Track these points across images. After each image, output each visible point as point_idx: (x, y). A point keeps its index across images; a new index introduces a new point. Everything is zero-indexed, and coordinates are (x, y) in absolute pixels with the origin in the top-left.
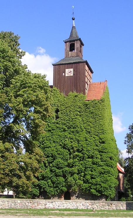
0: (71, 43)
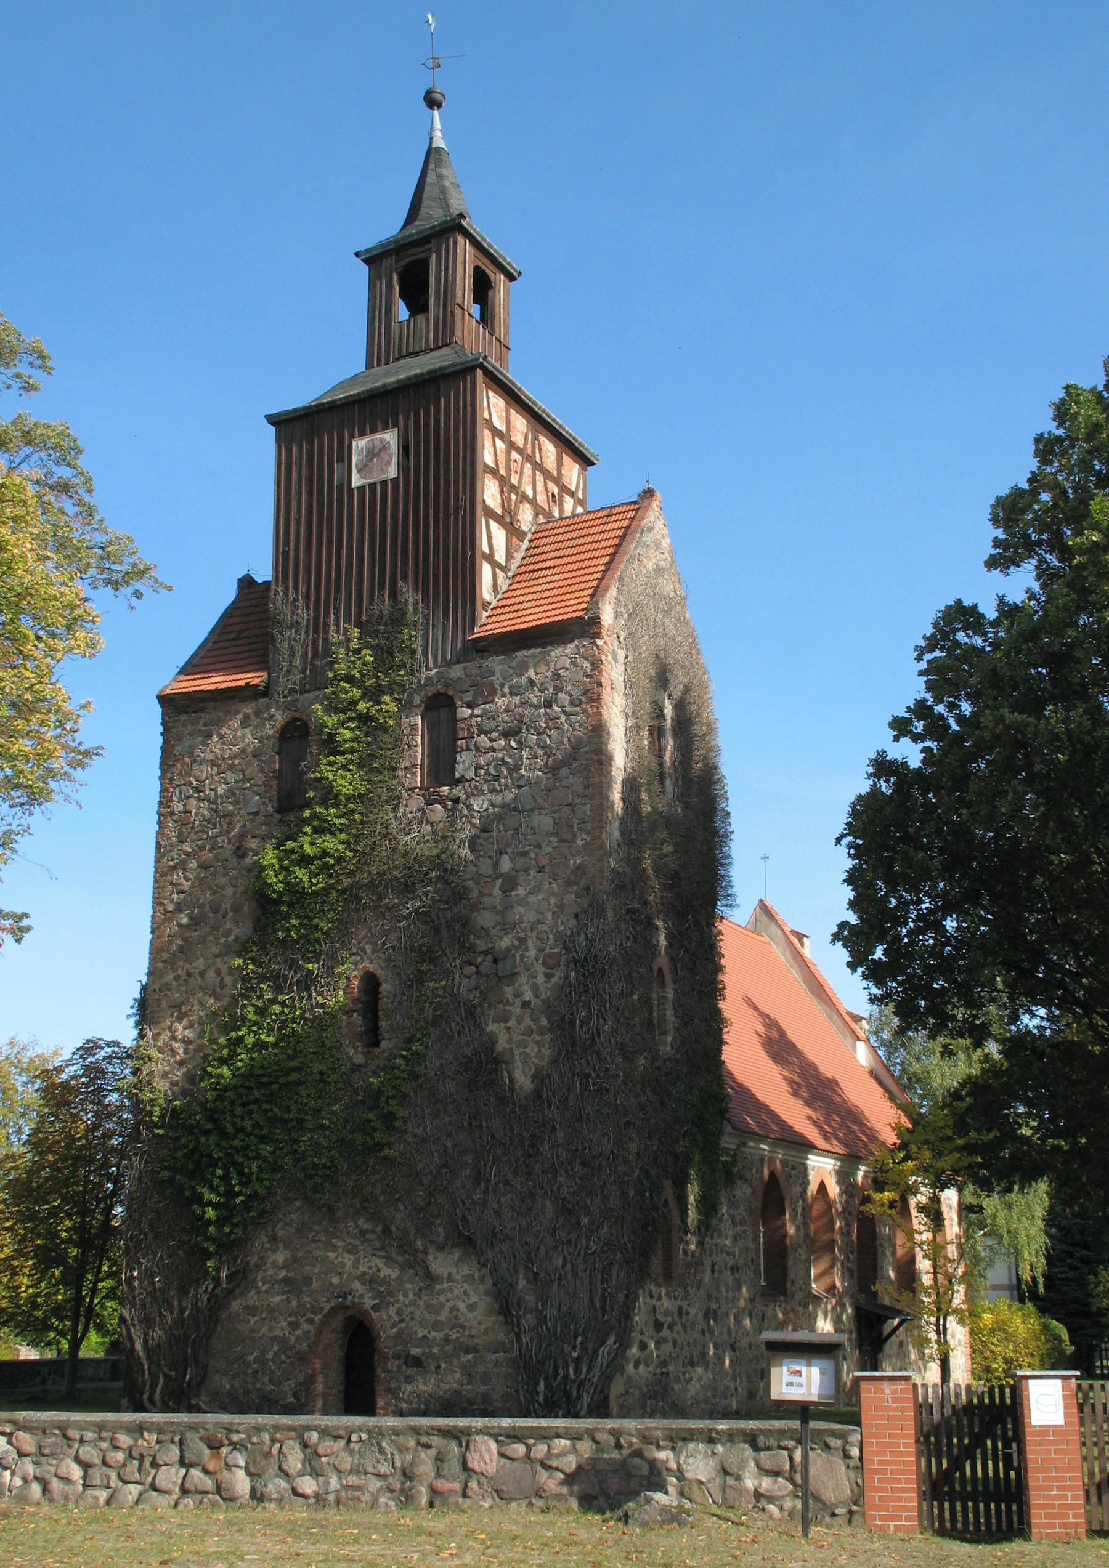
0: (403, 263)
